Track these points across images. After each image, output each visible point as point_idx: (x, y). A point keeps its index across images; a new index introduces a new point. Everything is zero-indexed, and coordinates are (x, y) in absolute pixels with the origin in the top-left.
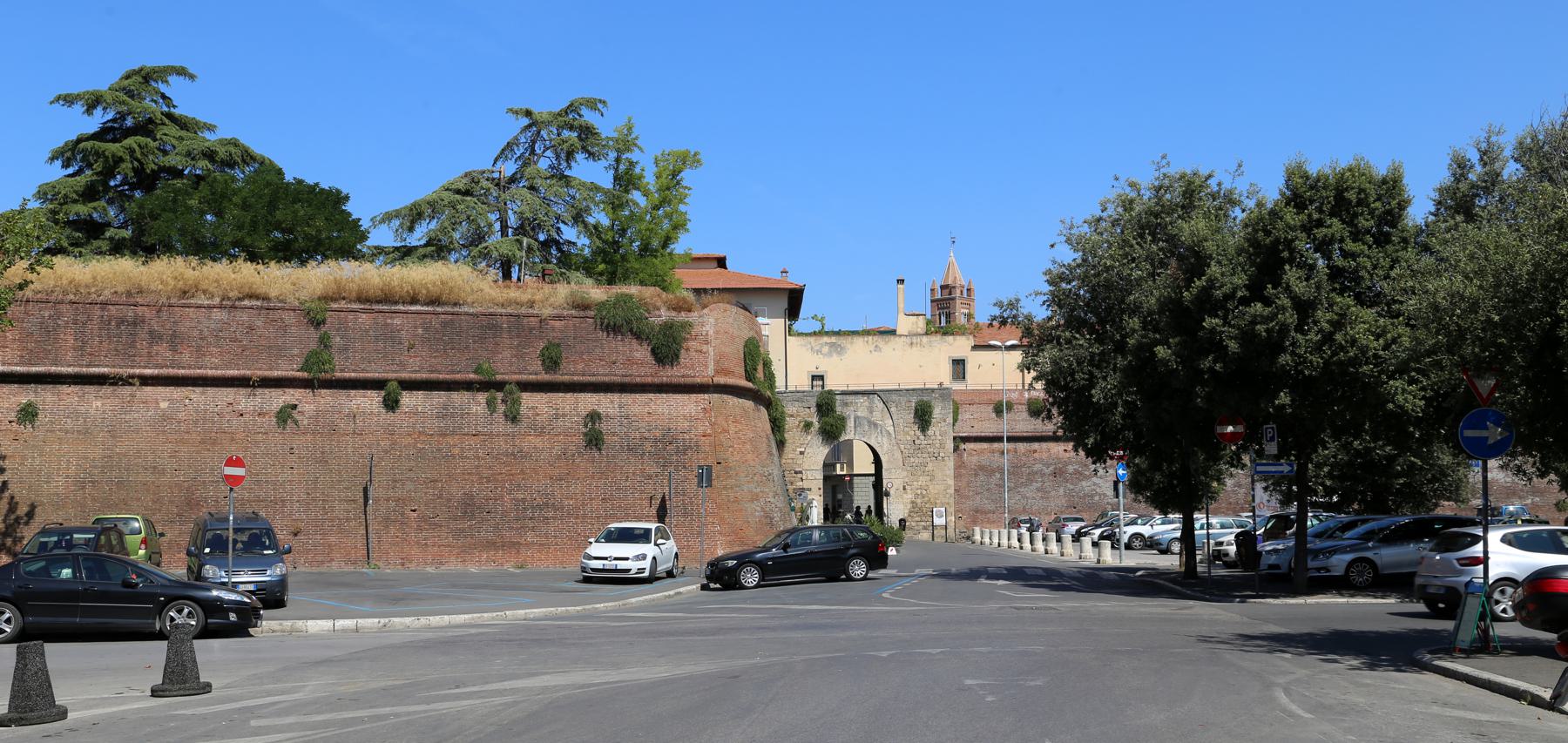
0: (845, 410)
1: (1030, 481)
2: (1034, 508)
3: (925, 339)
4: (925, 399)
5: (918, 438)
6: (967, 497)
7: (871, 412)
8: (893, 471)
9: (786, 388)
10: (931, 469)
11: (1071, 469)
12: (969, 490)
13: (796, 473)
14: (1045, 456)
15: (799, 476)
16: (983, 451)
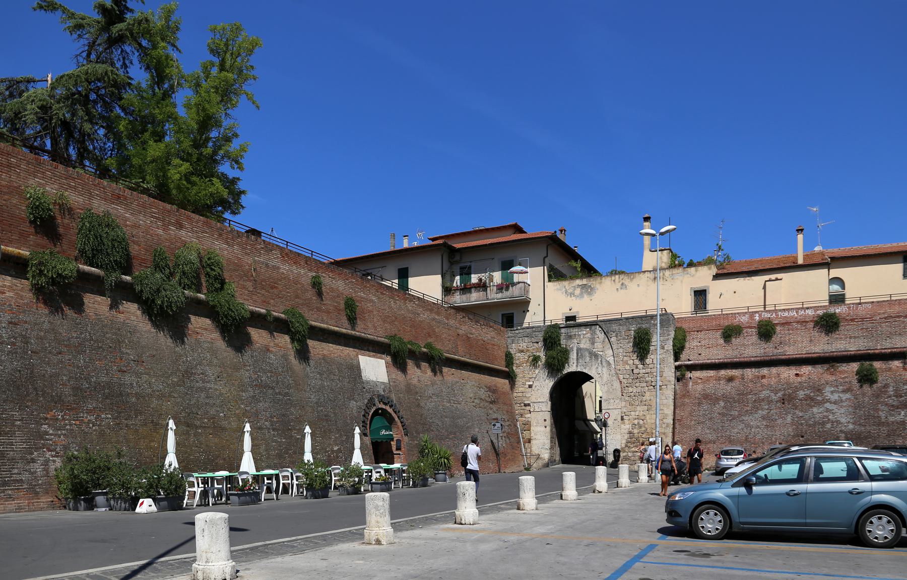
1: (756, 409)
2: (758, 437)
3: (667, 273)
4: (644, 326)
5: (637, 368)
6: (689, 427)
7: (593, 343)
8: (612, 401)
10: (648, 398)
11: (801, 394)
12: (691, 421)
13: (525, 405)
14: (773, 381)
15: (528, 408)
16: (708, 379)
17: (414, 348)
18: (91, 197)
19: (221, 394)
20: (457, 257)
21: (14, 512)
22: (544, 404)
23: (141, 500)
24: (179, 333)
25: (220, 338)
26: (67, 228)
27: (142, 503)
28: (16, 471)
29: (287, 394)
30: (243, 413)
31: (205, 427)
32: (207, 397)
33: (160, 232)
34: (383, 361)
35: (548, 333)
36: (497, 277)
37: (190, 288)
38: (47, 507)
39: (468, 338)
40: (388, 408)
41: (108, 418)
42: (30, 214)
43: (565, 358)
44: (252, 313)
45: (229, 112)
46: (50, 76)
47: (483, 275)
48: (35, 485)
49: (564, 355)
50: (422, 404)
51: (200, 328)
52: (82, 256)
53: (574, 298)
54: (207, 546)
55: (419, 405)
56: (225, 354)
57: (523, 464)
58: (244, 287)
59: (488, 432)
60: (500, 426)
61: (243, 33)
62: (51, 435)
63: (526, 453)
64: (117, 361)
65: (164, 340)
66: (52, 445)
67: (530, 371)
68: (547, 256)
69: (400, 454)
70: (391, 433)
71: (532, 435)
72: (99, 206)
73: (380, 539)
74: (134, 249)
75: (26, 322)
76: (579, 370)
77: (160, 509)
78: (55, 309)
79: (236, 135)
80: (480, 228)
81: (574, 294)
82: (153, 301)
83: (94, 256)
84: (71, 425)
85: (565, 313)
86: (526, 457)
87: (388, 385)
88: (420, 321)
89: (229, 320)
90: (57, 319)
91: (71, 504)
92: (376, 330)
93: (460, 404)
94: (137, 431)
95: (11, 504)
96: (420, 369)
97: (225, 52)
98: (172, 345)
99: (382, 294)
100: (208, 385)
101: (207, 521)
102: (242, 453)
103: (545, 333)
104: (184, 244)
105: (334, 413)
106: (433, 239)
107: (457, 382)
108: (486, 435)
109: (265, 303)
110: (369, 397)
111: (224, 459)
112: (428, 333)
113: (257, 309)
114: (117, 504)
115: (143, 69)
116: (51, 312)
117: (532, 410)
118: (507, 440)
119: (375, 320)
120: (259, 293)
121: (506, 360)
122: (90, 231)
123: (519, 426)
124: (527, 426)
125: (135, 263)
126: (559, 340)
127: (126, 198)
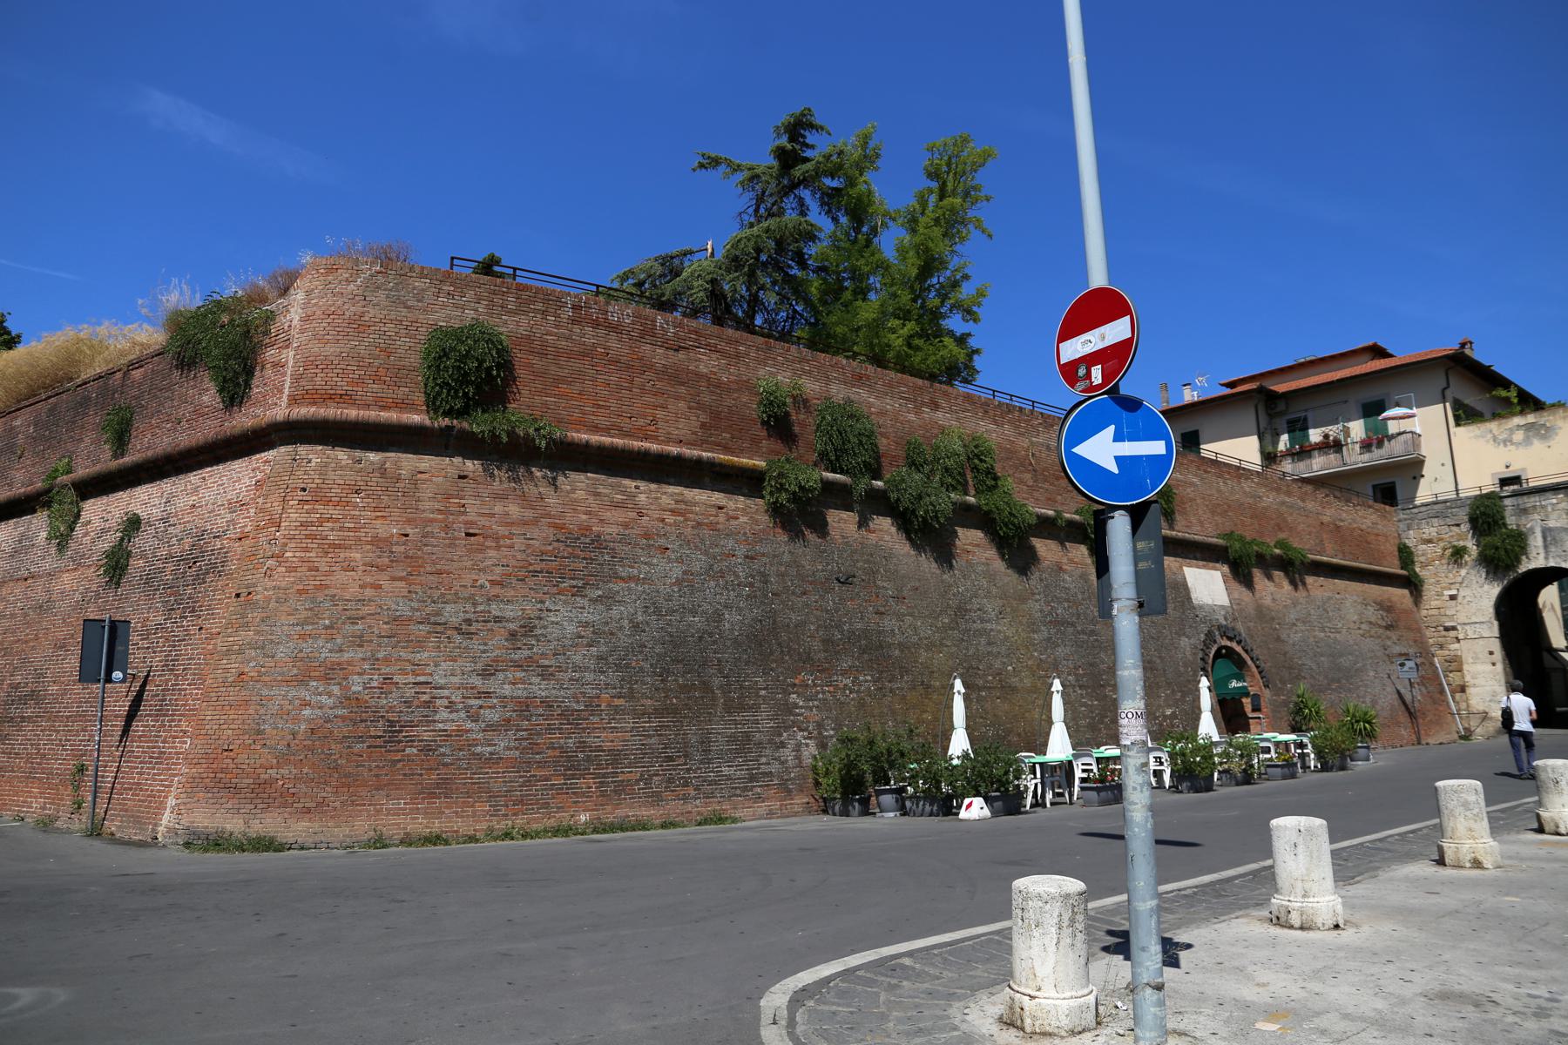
0: (1523, 520)
9: (1457, 494)
13: (1447, 629)
15: (1452, 634)
17: (1263, 550)
18: (828, 380)
19: (1006, 638)
20: (1281, 406)
21: (765, 819)
22: (1485, 626)
23: (967, 801)
24: (944, 553)
25: (996, 557)
26: (803, 425)
27: (970, 805)
28: (764, 760)
29: (1092, 633)
30: (1038, 665)
31: (990, 688)
32: (989, 644)
33: (912, 417)
34: (1218, 573)
35: (1478, 507)
36: (1357, 429)
37: (955, 489)
38: (803, 811)
39: (1338, 527)
40: (1234, 645)
41: (867, 681)
42: (763, 412)
43: (1519, 546)
44: (1039, 516)
45: (955, 248)
46: (710, 243)
47: (1330, 428)
48: (787, 780)
49: (1519, 542)
50: (1284, 636)
51: (970, 544)
52: (822, 460)
53: (1511, 447)
54: (1304, 871)
55: (1278, 639)
56: (1007, 579)
57: (1454, 729)
58: (1021, 482)
59: (1389, 677)
60: (1414, 666)
61: (971, 145)
62: (802, 707)
63: (1458, 710)
64: (872, 599)
65: (927, 565)
66: (803, 722)
67: (1450, 572)
68: (1448, 387)
69: (1259, 718)
70: (1245, 684)
71: (1468, 678)
72: (838, 392)
73: (1481, 858)
74: (883, 443)
75: (763, 555)
76: (1552, 564)
77: (995, 814)
78: (796, 535)
79: (966, 277)
80: (1308, 359)
81: (1511, 441)
82: (913, 512)
83: (837, 459)
84: (823, 693)
85: (1499, 473)
86: (1460, 718)
87: (1231, 611)
88: (1263, 508)
89: (1011, 529)
90: (798, 548)
91: (837, 808)
92: (1202, 526)
93: (1339, 632)
94: (904, 697)
95: (761, 807)
96: (1273, 581)
97: (948, 173)
98: (938, 572)
99: (1206, 472)
100: (989, 626)
101: (1302, 830)
102: (1050, 723)
103: (1471, 508)
104: (943, 430)
105: (1160, 657)
106: (1231, 385)
107: (1330, 598)
108: (1387, 681)
109: (1050, 501)
110: (1205, 629)
111: (1019, 735)
112: (1278, 525)
113: (1043, 511)
114: (918, 806)
115: (823, 213)
116: (791, 539)
117: (1461, 636)
118: (1423, 689)
119: (1200, 512)
120: (1041, 488)
121: (1400, 557)
122: (832, 427)
123: (1438, 665)
124: (1455, 663)
125: (885, 461)
126: (1503, 518)
127: (868, 378)
